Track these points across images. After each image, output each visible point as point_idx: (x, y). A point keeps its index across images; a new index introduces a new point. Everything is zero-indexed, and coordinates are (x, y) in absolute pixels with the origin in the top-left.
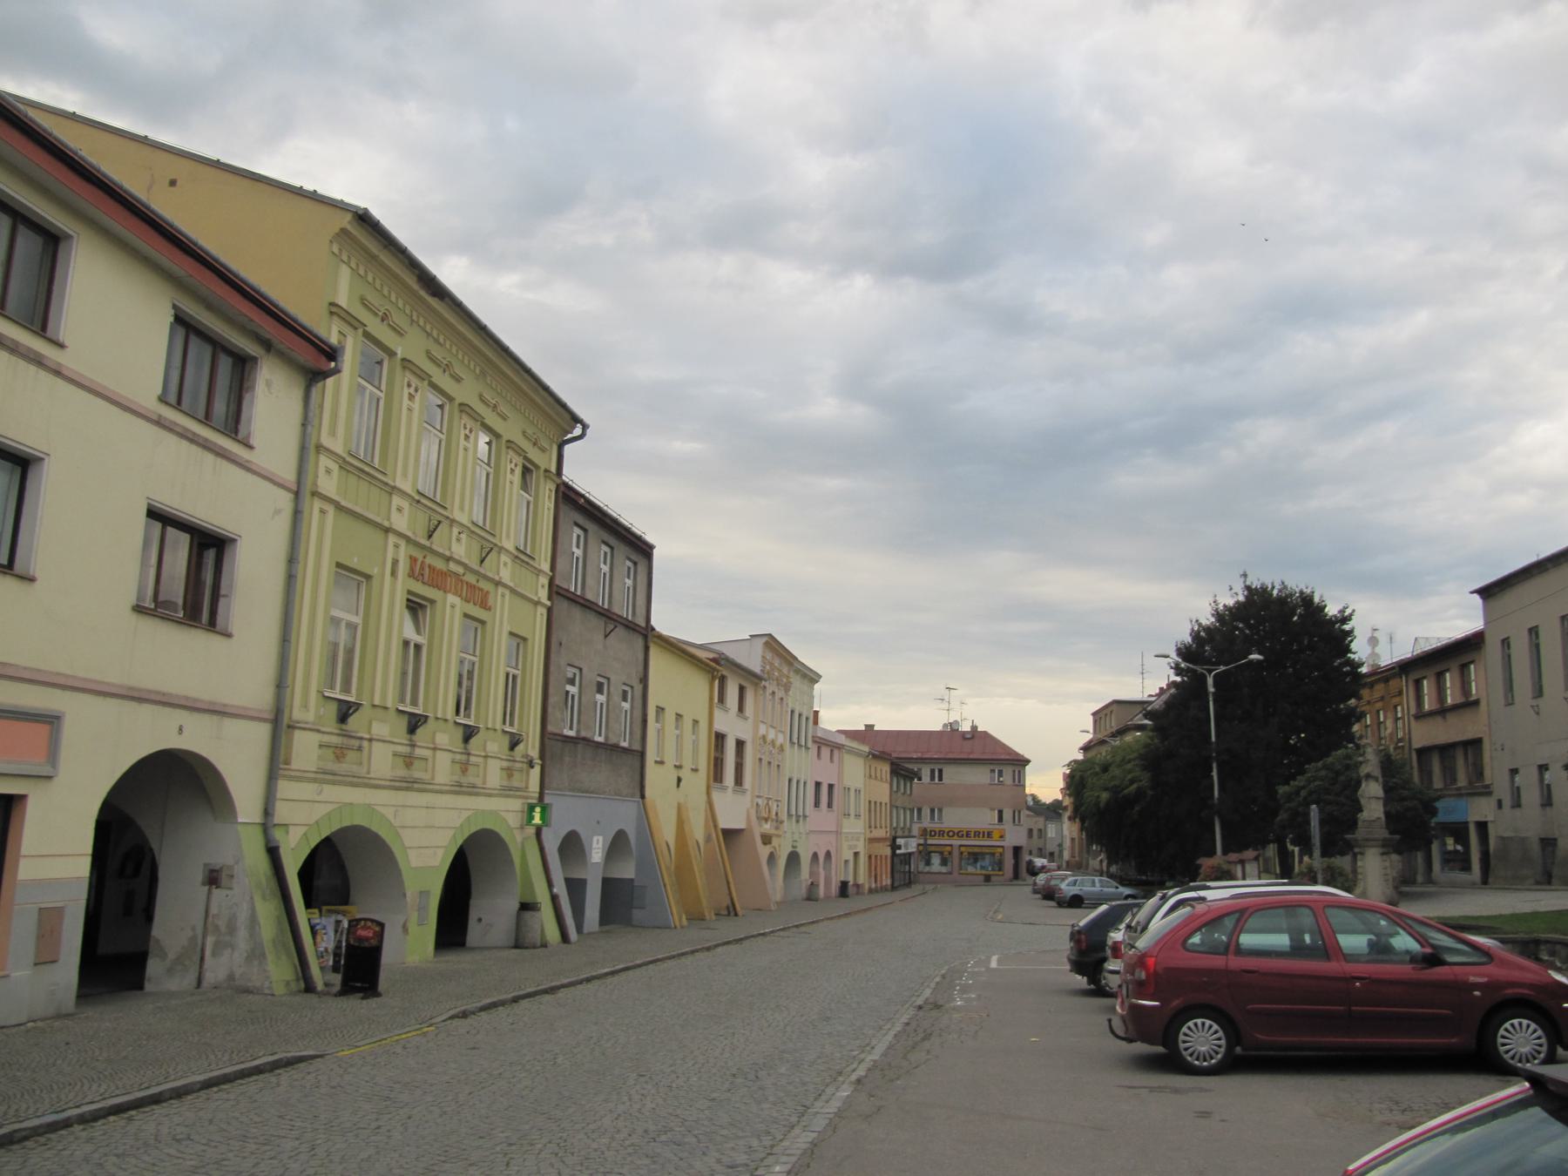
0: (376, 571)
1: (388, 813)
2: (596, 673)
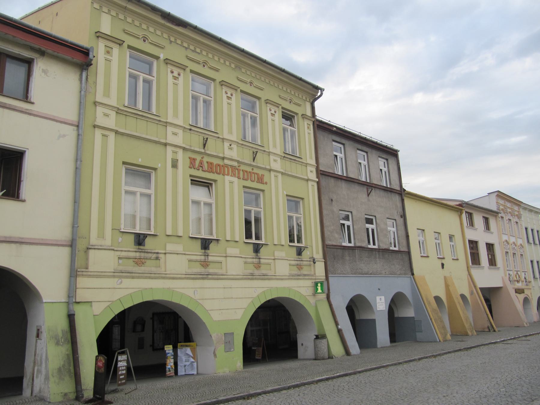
0: (160, 165)
1: (190, 293)
2: (364, 214)
